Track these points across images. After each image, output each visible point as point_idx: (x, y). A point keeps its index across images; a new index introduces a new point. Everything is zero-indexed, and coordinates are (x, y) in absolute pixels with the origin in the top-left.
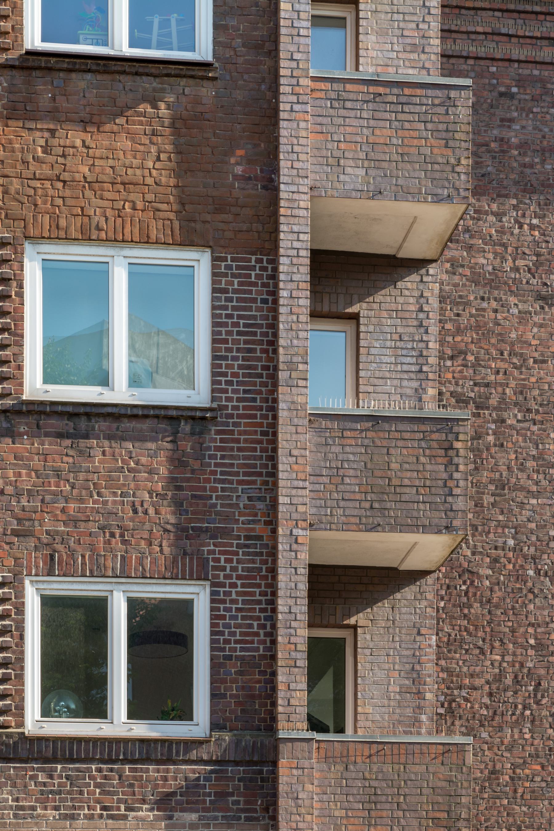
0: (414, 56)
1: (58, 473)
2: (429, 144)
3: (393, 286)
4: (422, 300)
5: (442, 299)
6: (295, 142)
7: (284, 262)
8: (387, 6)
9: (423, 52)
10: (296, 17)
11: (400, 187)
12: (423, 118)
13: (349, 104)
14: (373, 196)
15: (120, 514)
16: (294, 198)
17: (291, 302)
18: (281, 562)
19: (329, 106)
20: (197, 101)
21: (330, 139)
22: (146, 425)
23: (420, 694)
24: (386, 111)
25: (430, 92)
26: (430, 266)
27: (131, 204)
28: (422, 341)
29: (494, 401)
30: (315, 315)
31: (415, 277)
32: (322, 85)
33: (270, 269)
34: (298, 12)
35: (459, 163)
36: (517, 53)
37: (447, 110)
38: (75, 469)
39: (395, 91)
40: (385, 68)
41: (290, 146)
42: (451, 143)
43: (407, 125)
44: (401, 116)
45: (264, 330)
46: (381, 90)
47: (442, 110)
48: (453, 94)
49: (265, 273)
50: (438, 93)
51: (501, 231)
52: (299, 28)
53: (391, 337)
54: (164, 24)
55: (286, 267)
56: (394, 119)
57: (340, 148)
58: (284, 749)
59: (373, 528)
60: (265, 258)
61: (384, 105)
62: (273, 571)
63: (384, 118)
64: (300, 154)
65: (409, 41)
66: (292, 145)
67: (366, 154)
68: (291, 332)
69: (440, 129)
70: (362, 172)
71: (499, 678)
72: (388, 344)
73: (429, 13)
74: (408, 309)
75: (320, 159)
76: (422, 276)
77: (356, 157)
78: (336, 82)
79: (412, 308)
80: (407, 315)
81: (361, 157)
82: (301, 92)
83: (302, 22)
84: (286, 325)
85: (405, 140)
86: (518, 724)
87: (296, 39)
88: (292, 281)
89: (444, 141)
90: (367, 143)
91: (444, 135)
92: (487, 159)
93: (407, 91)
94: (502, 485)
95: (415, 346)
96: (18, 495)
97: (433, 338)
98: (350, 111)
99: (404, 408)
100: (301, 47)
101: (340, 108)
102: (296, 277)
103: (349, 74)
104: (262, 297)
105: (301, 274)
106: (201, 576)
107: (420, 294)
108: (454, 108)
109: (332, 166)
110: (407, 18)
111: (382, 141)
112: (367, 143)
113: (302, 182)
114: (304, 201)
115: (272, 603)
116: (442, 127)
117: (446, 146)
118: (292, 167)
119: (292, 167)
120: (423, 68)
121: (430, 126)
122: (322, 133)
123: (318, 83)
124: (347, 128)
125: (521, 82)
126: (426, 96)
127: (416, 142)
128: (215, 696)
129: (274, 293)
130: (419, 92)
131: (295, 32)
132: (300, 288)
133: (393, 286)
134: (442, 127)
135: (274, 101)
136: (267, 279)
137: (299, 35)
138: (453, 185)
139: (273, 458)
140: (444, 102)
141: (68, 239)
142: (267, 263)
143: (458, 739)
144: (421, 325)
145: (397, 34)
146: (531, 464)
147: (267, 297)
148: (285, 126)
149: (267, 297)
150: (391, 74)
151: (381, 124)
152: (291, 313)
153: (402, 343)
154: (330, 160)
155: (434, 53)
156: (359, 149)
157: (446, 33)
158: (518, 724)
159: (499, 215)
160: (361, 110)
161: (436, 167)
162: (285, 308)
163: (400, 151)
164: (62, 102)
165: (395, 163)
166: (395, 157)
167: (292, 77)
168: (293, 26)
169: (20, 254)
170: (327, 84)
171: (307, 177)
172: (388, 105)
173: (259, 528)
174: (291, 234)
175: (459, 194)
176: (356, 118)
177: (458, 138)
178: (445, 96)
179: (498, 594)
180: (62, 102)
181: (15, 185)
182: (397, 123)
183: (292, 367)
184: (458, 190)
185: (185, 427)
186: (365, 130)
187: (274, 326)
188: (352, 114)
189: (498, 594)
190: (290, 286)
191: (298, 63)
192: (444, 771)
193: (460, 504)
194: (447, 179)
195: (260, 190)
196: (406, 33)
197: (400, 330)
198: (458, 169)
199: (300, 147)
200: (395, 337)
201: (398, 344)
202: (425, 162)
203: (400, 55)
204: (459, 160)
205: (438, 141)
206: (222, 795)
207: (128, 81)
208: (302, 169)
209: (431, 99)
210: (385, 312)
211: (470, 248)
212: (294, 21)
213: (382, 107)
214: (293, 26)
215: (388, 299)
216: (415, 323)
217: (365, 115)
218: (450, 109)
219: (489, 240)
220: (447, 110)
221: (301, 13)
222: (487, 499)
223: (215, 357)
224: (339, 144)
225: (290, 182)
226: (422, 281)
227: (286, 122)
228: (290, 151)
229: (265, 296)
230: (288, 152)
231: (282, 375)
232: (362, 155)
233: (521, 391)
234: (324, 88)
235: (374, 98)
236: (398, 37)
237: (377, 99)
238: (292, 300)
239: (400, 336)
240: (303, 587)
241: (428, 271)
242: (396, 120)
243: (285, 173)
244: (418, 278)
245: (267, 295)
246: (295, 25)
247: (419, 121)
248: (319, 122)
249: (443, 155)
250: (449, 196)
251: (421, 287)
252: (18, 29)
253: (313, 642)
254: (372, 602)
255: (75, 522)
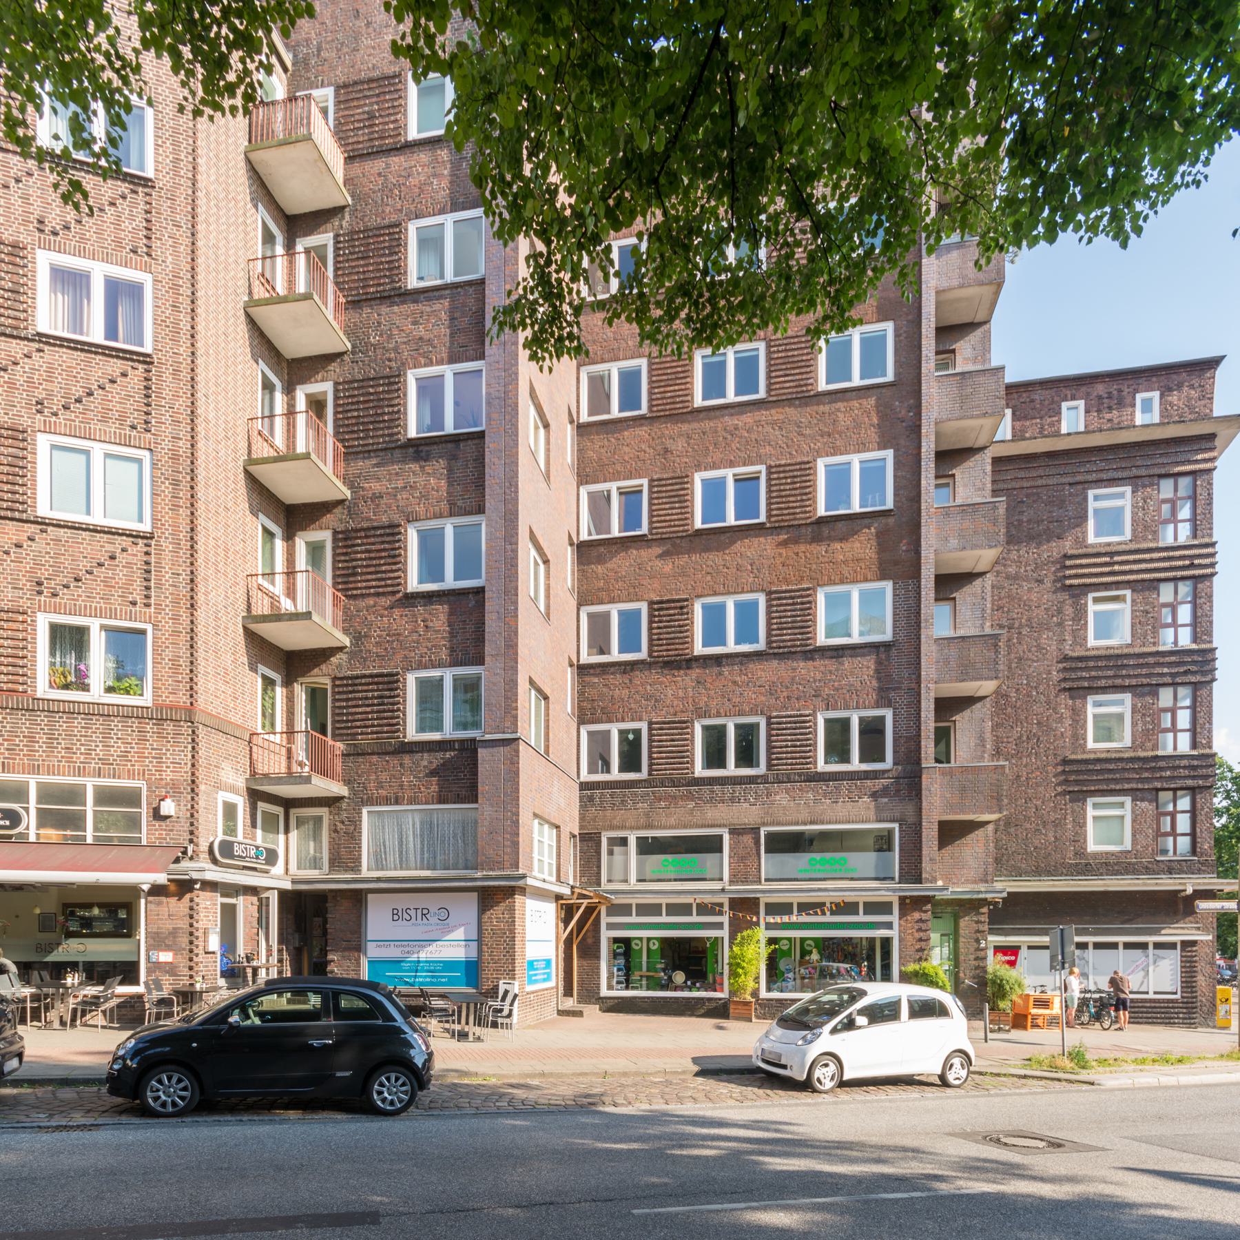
1: (830, 672)
5: (993, 587)
7: (923, 582)
15: (707, 295)
18: (923, 697)
20: (887, 524)
22: (866, 650)
23: (984, 746)
29: (1016, 625)
30: (937, 600)
36: (1025, 484)
38: (837, 670)
51: (1019, 557)
54: (874, 498)
58: (924, 771)
59: (963, 681)
62: (919, 702)
71: (1020, 738)
86: (1029, 756)
92: (1012, 529)
94: (1020, 659)
96: (815, 681)
99: (476, 1004)
103: (952, 504)
106: (889, 705)
114: (932, 556)
115: (919, 714)
125: (1027, 496)
128: (895, 752)
129: (919, 594)
139: (919, 657)
141: (835, 584)
143: (1001, 763)
146: (1034, 649)
150: (970, 501)
157: (994, 482)
158: (1029, 756)
159: (1018, 551)
164: (833, 533)
169: (815, 591)
173: (913, 685)
179: (1019, 704)
180: (833, 533)
181: (814, 566)
183: (927, 621)
185: (882, 649)
187: (919, 606)
189: (1019, 704)
192: (995, 776)
193: (1001, 667)
206: (898, 791)
207: (859, 522)
211: (1005, 565)
219: (1014, 561)
222: (1014, 665)
223: (895, 621)
231: (923, 625)
233: (1029, 620)
240: (932, 706)
252: (815, 509)
253: (937, 729)
254: (962, 711)
255: (837, 690)
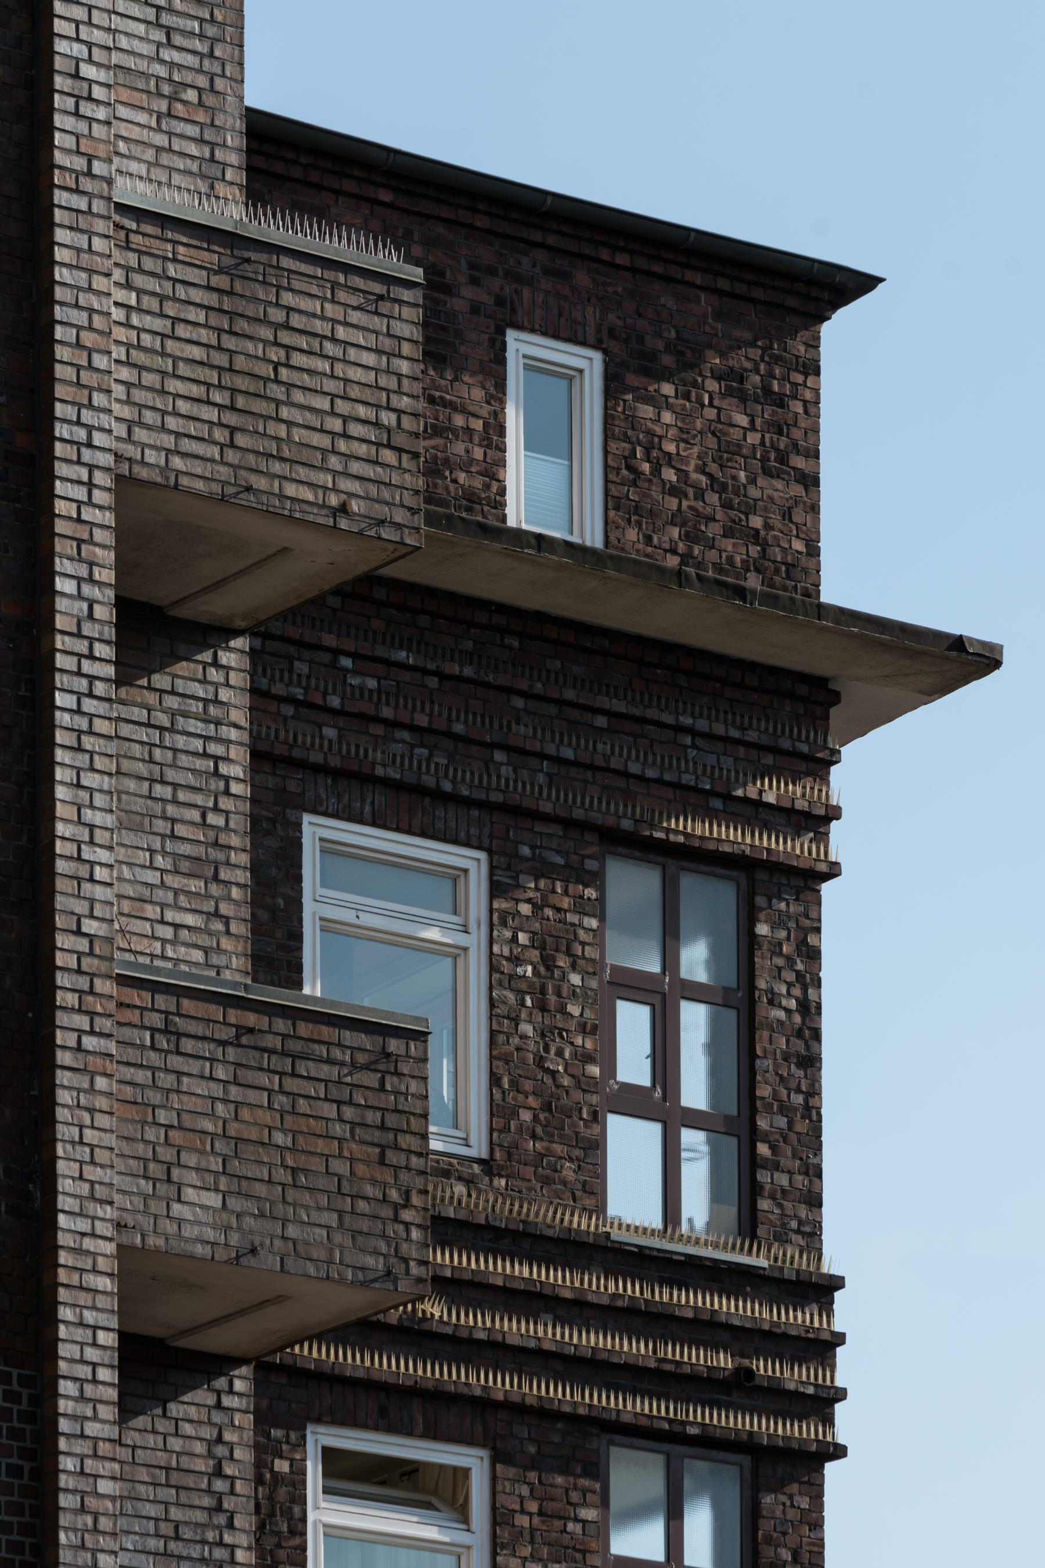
0: (195, 885)
2: (346, 1154)
3: (159, 1411)
4: (221, 1451)
6: (87, 1121)
8: (141, 764)
9: (216, 878)
10: (87, 838)
11: (291, 1244)
12: (334, 1093)
13: (188, 1045)
14: (238, 1257)
16: (85, 1247)
17: (84, 1485)
19: (148, 1043)
21: (150, 1119)
24: (261, 1069)
25: (348, 1037)
26: (236, 1372)
27: (169, 1415)
28: (221, 1544)
31: (203, 1396)
32: (135, 996)
33: (25, 1399)
34: (92, 827)
35: (407, 1205)
37: (382, 1082)
39: (281, 1025)
40: (138, 904)
41: (77, 1129)
42: (391, 1157)
43: (302, 1105)
44: (291, 1085)
45: (15, 1537)
46: (251, 1019)
47: (371, 1079)
48: (394, 1045)
49: (16, 1408)
50: (363, 1040)
52: (92, 864)
53: (156, 1528)
55: (71, 1403)
56: (277, 1088)
57: (171, 1141)
60: (15, 1372)
61: (257, 1054)
63: (257, 1083)
64: (97, 1150)
65: (185, 849)
66: (81, 1127)
67: (224, 1161)
68: (82, 1553)
69: (369, 1121)
70: (213, 1200)
72: (153, 1544)
73: (227, 792)
74: (192, 1467)
75: (131, 1161)
76: (219, 1393)
77: (203, 1164)
78: (163, 993)
79: (200, 1465)
80: (190, 1481)
81: (213, 1167)
82: (99, 1009)
83: (98, 850)
84: (71, 1535)
85: (300, 1139)
87: (86, 887)
88: (82, 1436)
89: (377, 1150)
90: (224, 1135)
91: (377, 1136)
93: (304, 1029)
95: (206, 1554)
97: (243, 1540)
98: (191, 1061)
100: (97, 906)
101: (171, 1052)
102: (92, 1429)
104: (10, 1461)
105: (103, 1422)
107: (215, 1435)
108: (395, 1079)
109: (155, 1181)
110: (182, 796)
111: (254, 1136)
112: (224, 1135)
113: (100, 1213)
116: (373, 1117)
117: (382, 1162)
118: (81, 1178)
119: (81, 1178)
120: (216, 914)
121: (348, 1112)
122: (135, 1103)
123: (126, 990)
124: (185, 1098)
126: (339, 1045)
127: (321, 1146)
130: (326, 1032)
131: (84, 871)
132: (100, 1453)
133: (159, 1411)
134: (373, 1117)
135: (30, 1015)
136: (19, 1421)
137: (91, 880)
138: (396, 1250)
140: (376, 1062)
142: (20, 1384)
144: (219, 1508)
145: (161, 831)
147: (21, 1462)
148: (66, 1083)
149: (21, 1462)
151: (252, 1096)
152: (83, 1509)
153: (181, 1544)
154: (152, 1166)
155: (238, 885)
156: (208, 1148)
160: (212, 1060)
161: (362, 1206)
162: (70, 1496)
163: (290, 1162)
165: (280, 1188)
166: (282, 1175)
167: (79, 971)
168: (79, 858)
170: (144, 993)
171: (111, 1203)
172: (266, 1055)
174: (80, 1331)
175: (407, 1272)
176: (202, 1077)
177: (404, 1147)
178: (378, 1049)
182: (284, 1099)
184: (406, 1261)
186: (220, 1107)
188: (194, 1067)
190: (82, 1447)
191: (91, 943)
194: (384, 1236)
195: (4, 1216)
196: (181, 830)
197: (175, 1513)
198: (407, 1215)
199: (96, 1133)
200: (166, 1529)
201: (172, 1545)
202: (339, 1192)
203: (169, 879)
204: (407, 1194)
205: (364, 1147)
208: (101, 1183)
209: (349, 1052)
210: (144, 1470)
212: (83, 846)
213: (251, 1057)
214: (79, 858)
215: (151, 1440)
216: (207, 1501)
217: (221, 1073)
218: (388, 1079)
220: (382, 1082)
221: (98, 832)
224: (171, 1133)
225: (77, 1210)
226: (219, 1405)
227: (68, 1074)
228: (77, 1139)
229: (14, 1460)
230: (73, 1143)
232: (216, 1164)
234: (138, 1003)
235: (238, 1036)
236: (163, 836)
237: (244, 1040)
238: (83, 1479)
239: (176, 1528)
241: (231, 1384)
242: (282, 1091)
243: (67, 1189)
244: (211, 1400)
245: (20, 1457)
246: (85, 856)
247: (326, 1099)
248: (128, 1077)
249: (374, 1182)
250: (389, 1273)
251: (218, 1417)
